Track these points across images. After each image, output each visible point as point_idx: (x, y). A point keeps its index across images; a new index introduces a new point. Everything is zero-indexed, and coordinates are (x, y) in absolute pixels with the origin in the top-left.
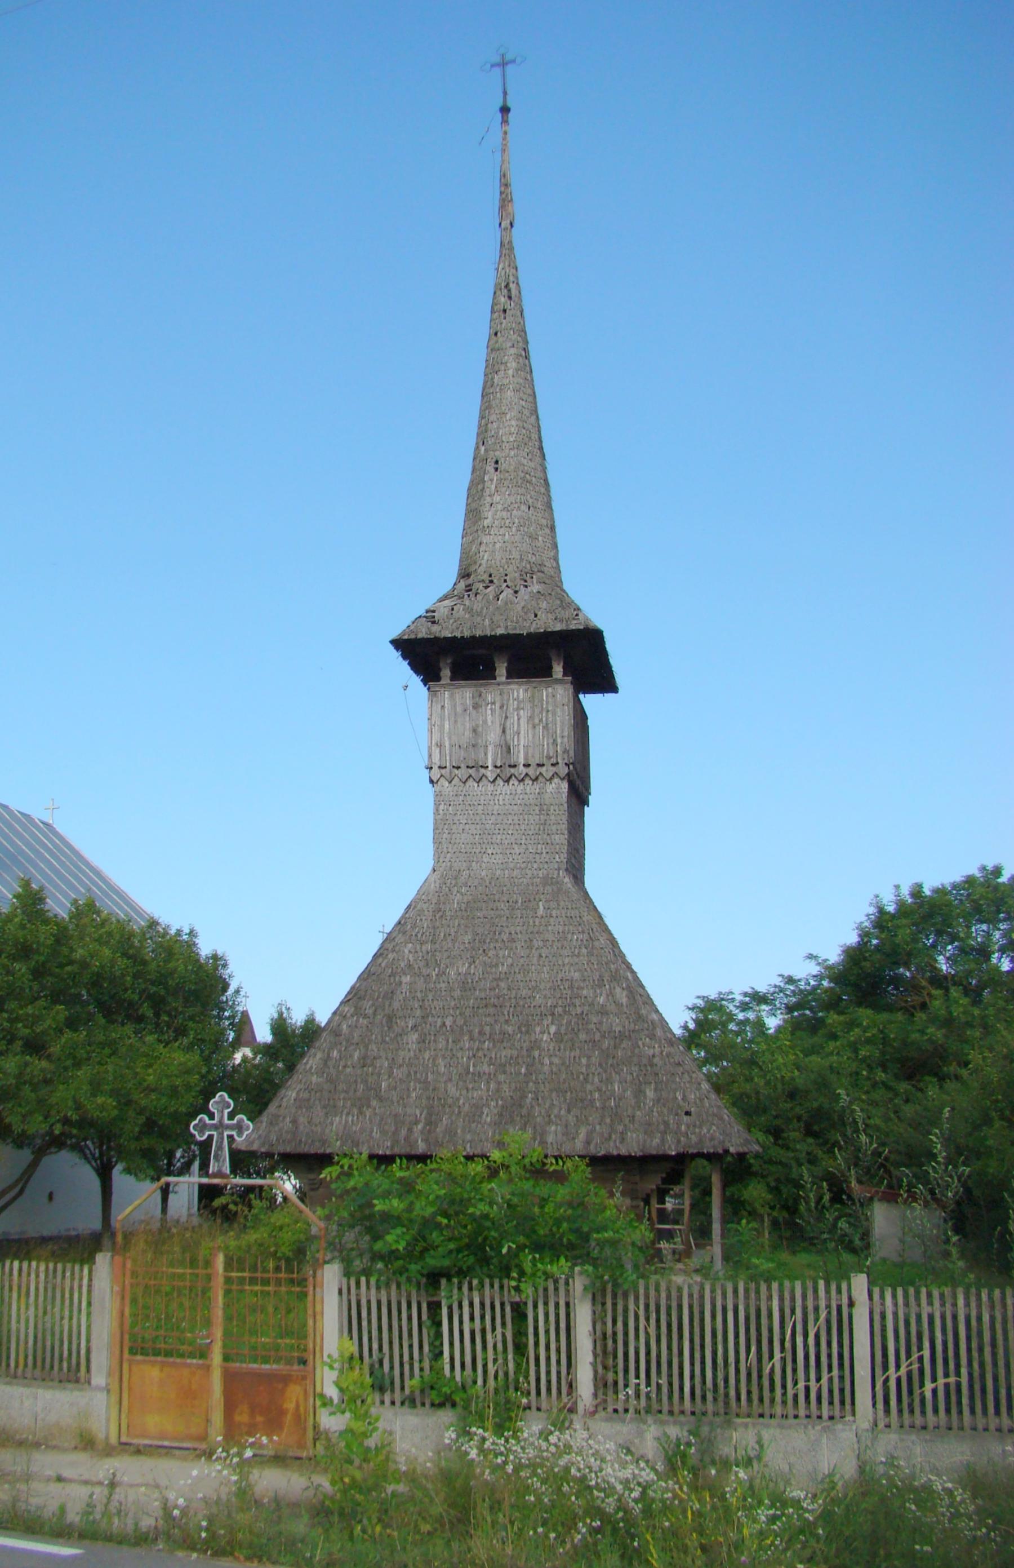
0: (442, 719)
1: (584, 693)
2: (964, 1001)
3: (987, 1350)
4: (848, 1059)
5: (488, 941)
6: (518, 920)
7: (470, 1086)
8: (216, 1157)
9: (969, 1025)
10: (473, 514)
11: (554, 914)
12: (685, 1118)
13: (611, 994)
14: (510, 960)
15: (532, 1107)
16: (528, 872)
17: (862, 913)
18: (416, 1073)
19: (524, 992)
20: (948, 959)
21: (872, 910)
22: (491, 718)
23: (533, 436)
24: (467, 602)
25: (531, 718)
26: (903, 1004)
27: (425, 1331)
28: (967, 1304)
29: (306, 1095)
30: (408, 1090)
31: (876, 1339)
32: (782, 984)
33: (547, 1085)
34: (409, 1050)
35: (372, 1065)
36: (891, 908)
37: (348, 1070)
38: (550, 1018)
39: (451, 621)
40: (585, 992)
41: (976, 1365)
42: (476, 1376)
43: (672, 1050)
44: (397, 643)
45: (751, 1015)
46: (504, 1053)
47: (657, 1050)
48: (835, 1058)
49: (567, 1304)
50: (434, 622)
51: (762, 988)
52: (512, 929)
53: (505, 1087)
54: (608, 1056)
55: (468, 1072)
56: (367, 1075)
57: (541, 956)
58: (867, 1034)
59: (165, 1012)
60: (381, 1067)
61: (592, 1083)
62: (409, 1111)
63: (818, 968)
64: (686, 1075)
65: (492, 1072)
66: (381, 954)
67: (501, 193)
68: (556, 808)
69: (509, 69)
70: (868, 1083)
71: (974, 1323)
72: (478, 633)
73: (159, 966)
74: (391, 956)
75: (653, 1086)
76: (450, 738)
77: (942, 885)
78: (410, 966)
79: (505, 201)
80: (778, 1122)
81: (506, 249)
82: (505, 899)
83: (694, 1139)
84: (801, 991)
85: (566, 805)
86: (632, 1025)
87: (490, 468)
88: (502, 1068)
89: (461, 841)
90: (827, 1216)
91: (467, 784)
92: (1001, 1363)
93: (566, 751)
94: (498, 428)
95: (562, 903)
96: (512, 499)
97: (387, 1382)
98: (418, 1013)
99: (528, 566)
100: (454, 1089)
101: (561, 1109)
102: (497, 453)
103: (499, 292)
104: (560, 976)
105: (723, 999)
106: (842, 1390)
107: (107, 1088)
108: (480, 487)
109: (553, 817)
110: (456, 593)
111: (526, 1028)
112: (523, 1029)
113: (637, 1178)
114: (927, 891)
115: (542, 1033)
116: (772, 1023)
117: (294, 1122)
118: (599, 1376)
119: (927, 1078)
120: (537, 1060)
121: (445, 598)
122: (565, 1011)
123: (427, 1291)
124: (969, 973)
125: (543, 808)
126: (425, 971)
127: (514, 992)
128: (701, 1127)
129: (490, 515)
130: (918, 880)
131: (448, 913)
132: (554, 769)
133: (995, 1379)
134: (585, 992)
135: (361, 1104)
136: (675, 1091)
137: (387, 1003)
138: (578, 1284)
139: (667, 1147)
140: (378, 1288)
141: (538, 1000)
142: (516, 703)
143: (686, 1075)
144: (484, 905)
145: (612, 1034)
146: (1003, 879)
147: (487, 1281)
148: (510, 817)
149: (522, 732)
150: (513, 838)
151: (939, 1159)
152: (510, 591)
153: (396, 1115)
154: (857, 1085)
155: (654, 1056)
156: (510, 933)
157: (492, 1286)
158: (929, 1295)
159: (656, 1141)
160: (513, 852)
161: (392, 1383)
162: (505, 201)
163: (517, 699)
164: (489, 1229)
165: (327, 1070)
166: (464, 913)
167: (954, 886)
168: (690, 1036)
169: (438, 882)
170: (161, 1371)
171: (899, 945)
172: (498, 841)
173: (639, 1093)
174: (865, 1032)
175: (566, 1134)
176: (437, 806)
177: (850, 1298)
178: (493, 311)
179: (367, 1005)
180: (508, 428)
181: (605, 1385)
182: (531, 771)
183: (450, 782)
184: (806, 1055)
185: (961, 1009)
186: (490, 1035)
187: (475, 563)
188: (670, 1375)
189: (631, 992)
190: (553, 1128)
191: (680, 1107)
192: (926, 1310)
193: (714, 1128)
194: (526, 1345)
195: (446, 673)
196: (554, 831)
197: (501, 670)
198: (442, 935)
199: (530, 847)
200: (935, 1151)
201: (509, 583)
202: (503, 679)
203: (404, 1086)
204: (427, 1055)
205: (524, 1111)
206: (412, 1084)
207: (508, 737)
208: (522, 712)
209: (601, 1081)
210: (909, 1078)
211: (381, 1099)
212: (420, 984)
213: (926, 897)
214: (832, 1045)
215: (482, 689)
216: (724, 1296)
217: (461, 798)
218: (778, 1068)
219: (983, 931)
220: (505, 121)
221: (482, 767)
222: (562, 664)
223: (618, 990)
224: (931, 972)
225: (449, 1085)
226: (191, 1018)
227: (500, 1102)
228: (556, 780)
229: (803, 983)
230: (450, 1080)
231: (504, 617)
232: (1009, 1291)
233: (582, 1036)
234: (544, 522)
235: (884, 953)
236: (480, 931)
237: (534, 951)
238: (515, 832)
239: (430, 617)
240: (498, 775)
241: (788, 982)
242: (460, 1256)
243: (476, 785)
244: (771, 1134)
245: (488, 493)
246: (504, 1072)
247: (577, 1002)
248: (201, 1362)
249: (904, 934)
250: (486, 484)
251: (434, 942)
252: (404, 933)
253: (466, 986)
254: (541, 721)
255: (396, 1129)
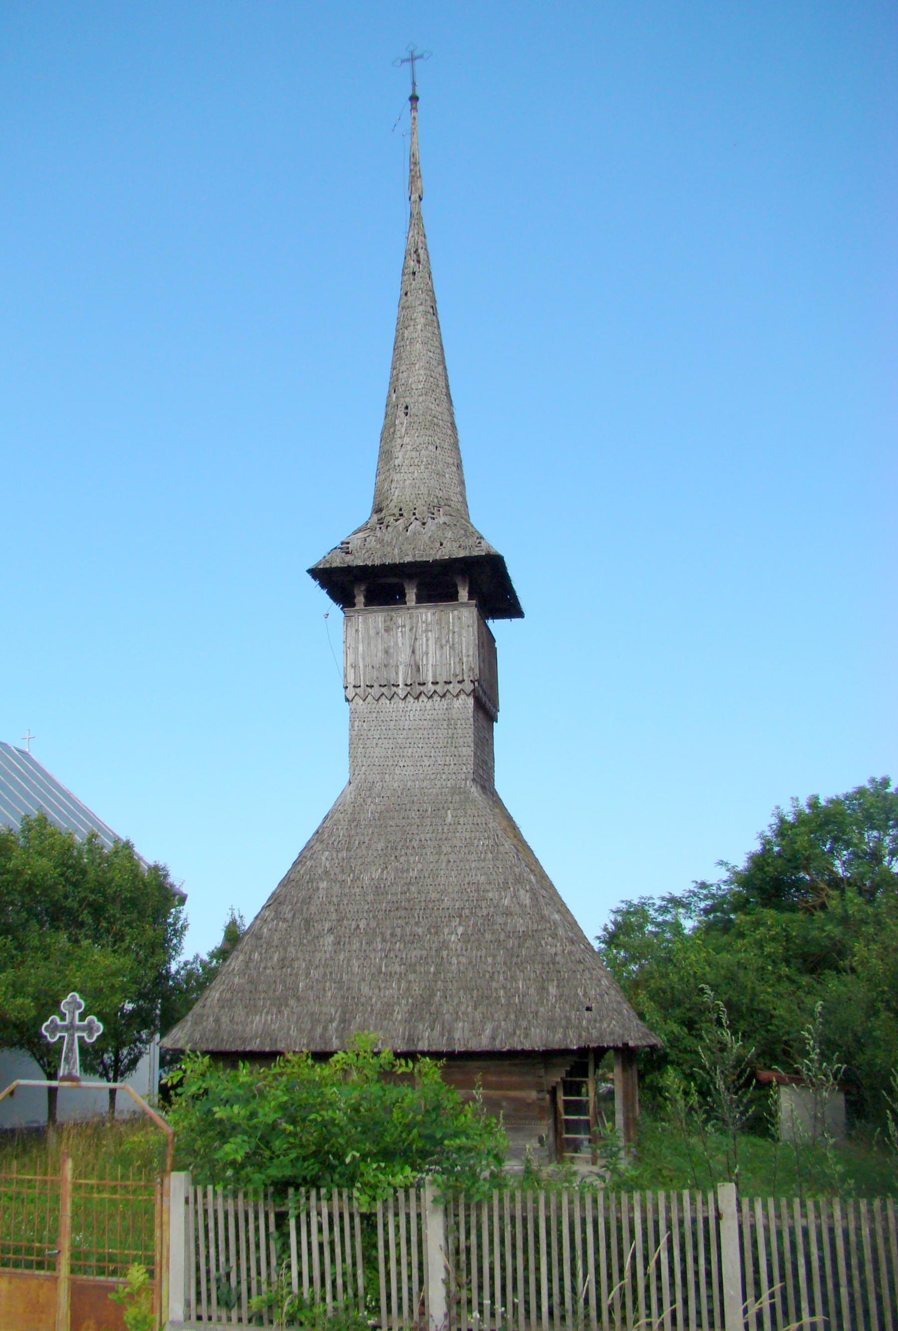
0: (357, 642)
1: (493, 618)
2: (859, 900)
3: (869, 1267)
4: (755, 955)
5: (399, 848)
6: (428, 828)
7: (383, 985)
8: (67, 1059)
9: (864, 922)
10: (386, 455)
11: (461, 820)
12: (587, 1013)
13: (515, 896)
14: (420, 866)
15: (441, 1004)
16: (436, 782)
17: (766, 824)
18: (331, 973)
19: (434, 896)
20: (844, 863)
21: (774, 820)
22: (401, 640)
23: (440, 383)
24: (379, 534)
25: (438, 639)
26: (804, 905)
27: (272, 1243)
28: (845, 1216)
29: (229, 995)
30: (324, 990)
31: (746, 1255)
32: (696, 890)
33: (454, 982)
34: (325, 952)
35: (291, 965)
36: (790, 818)
37: (268, 971)
38: (458, 919)
39: (364, 552)
40: (490, 895)
41: (856, 1284)
42: (325, 1292)
43: (574, 948)
44: (315, 573)
45: (668, 917)
46: (414, 953)
47: (559, 948)
48: (743, 955)
49: (419, 1216)
50: (347, 553)
51: (678, 893)
52: (423, 837)
53: (415, 986)
54: (512, 955)
55: (381, 972)
56: (286, 976)
57: (449, 861)
58: (772, 933)
59: (105, 918)
60: (299, 968)
61: (498, 982)
62: (324, 1009)
63: (728, 874)
64: (587, 972)
65: (403, 972)
66: (301, 861)
67: (411, 171)
68: (463, 722)
69: (417, 63)
70: (774, 976)
71: (853, 1238)
72: (388, 561)
73: (98, 876)
74: (309, 863)
75: (555, 983)
76: (364, 659)
77: (837, 796)
78: (326, 872)
79: (414, 177)
80: (690, 1014)
81: (416, 219)
82: (416, 809)
83: (595, 1033)
84: (713, 895)
85: (472, 719)
86: (535, 925)
87: (401, 413)
88: (412, 968)
89: (375, 755)
90: (696, 1119)
91: (380, 702)
92: (885, 1282)
93: (471, 669)
94: (408, 377)
95: (469, 811)
96: (421, 440)
97: (234, 1298)
98: (334, 916)
99: (435, 500)
100: (367, 988)
101: (468, 1006)
102: (407, 400)
103: (408, 258)
104: (467, 880)
105: (644, 903)
106: (711, 1312)
107: (30, 990)
108: (392, 430)
109: (460, 731)
110: (369, 526)
111: (435, 930)
112: (432, 931)
113: (542, 1072)
114: (822, 802)
115: (451, 933)
116: (689, 924)
117: (217, 1020)
118: (451, 1295)
119: (826, 971)
120: (445, 960)
121: (360, 530)
122: (471, 913)
123: (274, 1201)
124: (862, 876)
125: (451, 723)
126: (340, 877)
127: (424, 896)
128: (601, 1021)
129: (400, 455)
130: (814, 792)
131: (363, 823)
132: (460, 686)
133: (879, 1298)
134: (490, 895)
135: (280, 1003)
136: (576, 988)
137: (305, 908)
138: (429, 1194)
139: (569, 1041)
140: (225, 1197)
141: (447, 902)
142: (424, 625)
143: (587, 972)
144: (396, 814)
145: (516, 935)
146: (891, 790)
147: (335, 1191)
148: (420, 732)
149: (431, 652)
150: (423, 751)
151: (813, 1056)
152: (418, 523)
153: (312, 1014)
154: (763, 979)
155: (556, 954)
156: (420, 840)
157: (340, 1194)
158: (803, 1205)
159: (559, 1035)
160: (423, 764)
161: (239, 1298)
162: (414, 177)
163: (426, 622)
164: (336, 1135)
165: (249, 971)
166: (378, 823)
167: (847, 797)
168: (610, 937)
169: (353, 793)
170: (10, 1283)
171: (798, 850)
172: (409, 754)
173: (543, 989)
174: (769, 930)
175: (473, 1030)
176: (352, 722)
177: (717, 1209)
178: (403, 274)
179: (286, 910)
180: (417, 377)
181: (459, 1303)
182: (439, 689)
183: (364, 700)
184: (718, 953)
185: (856, 908)
186: (402, 936)
187: (387, 498)
188: (527, 1294)
189: (534, 894)
190: (460, 1024)
191: (581, 1003)
192: (799, 1223)
193: (614, 1022)
194: (376, 1258)
195: (360, 599)
196: (462, 744)
197: (411, 595)
198: (357, 843)
199: (439, 759)
200: (808, 1047)
201: (417, 516)
202: (413, 604)
203: (320, 986)
204: (342, 957)
205: (433, 1009)
206: (328, 984)
207: (417, 658)
208: (430, 633)
209: (506, 979)
210: (812, 971)
211: (298, 999)
212: (336, 889)
213: (822, 807)
214: (740, 942)
215: (393, 614)
216: (583, 1208)
217: (374, 715)
218: (691, 965)
219: (875, 837)
220: (414, 109)
221: (393, 685)
222: (467, 589)
223: (522, 892)
224: (829, 876)
225: (363, 984)
226: (129, 924)
227: (410, 1000)
228: (463, 696)
229: (714, 888)
230: (364, 980)
231: (413, 546)
232: (890, 1203)
233: (488, 936)
234: (451, 461)
235: (785, 859)
236: (392, 838)
237: (442, 856)
238: (424, 745)
239: (344, 546)
240: (409, 693)
241: (701, 888)
242: (306, 1164)
243: (388, 702)
244: (686, 1025)
245: (399, 435)
246: (415, 972)
247: (484, 904)
248: (48, 1273)
249: (802, 841)
250: (397, 428)
251: (348, 849)
252: (322, 842)
253: (379, 890)
254: (448, 641)
255: (312, 1027)
